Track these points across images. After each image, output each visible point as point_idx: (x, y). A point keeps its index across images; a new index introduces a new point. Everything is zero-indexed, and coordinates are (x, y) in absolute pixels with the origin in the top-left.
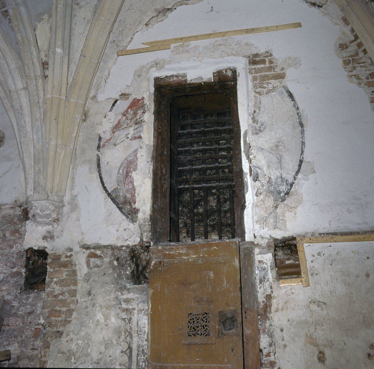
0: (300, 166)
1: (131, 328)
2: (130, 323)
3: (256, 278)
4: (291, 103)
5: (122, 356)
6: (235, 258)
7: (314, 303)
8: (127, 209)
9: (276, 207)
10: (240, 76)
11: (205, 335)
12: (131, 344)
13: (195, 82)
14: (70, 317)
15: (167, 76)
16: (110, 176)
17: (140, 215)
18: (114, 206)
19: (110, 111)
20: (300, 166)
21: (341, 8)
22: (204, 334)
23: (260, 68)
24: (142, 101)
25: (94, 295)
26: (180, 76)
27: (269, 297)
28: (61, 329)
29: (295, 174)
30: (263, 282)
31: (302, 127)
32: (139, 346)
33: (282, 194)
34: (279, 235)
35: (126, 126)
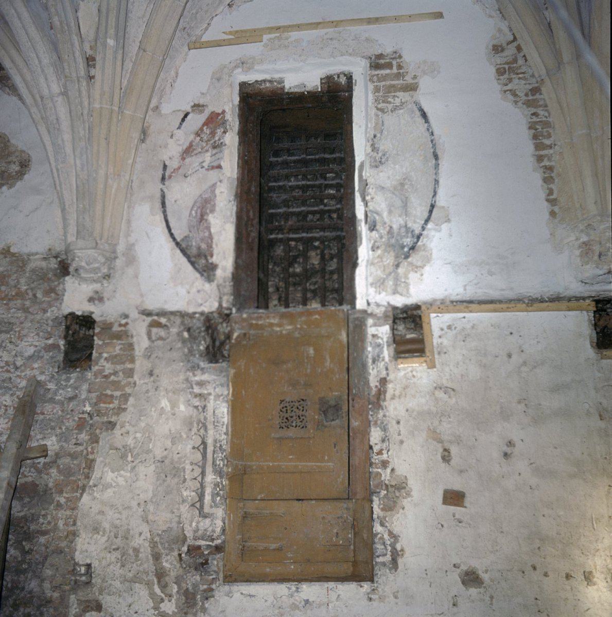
0: (431, 212)
1: (205, 419)
7: (441, 388)
9: (397, 266)
13: (296, 90)
15: (257, 81)
17: (219, 272)
20: (431, 212)
26: (275, 81)
27: (383, 381)
28: (113, 419)
32: (215, 441)
33: (406, 249)
34: (399, 301)
35: (200, 150)
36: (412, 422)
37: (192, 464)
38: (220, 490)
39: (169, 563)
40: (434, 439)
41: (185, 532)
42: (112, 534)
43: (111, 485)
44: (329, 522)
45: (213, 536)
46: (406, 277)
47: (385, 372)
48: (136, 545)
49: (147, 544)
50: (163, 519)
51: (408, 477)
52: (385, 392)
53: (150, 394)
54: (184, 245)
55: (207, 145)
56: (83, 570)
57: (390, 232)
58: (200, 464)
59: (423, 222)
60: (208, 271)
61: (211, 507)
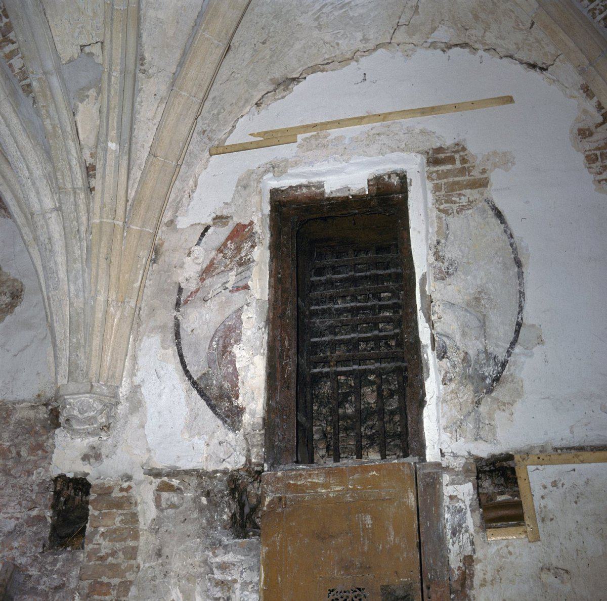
0: (517, 332)
3: (445, 527)
4: (499, 228)
6: (409, 491)
7: (549, 570)
8: (225, 408)
9: (478, 403)
13: (338, 195)
17: (246, 418)
18: (202, 403)
19: (198, 244)
20: (517, 332)
23: (445, 171)
25: (167, 556)
26: (314, 186)
27: (469, 561)
29: (508, 346)
31: (519, 267)
33: (488, 381)
34: (484, 450)
46: (491, 418)
52: (472, 576)
55: (231, 262)
57: (466, 359)
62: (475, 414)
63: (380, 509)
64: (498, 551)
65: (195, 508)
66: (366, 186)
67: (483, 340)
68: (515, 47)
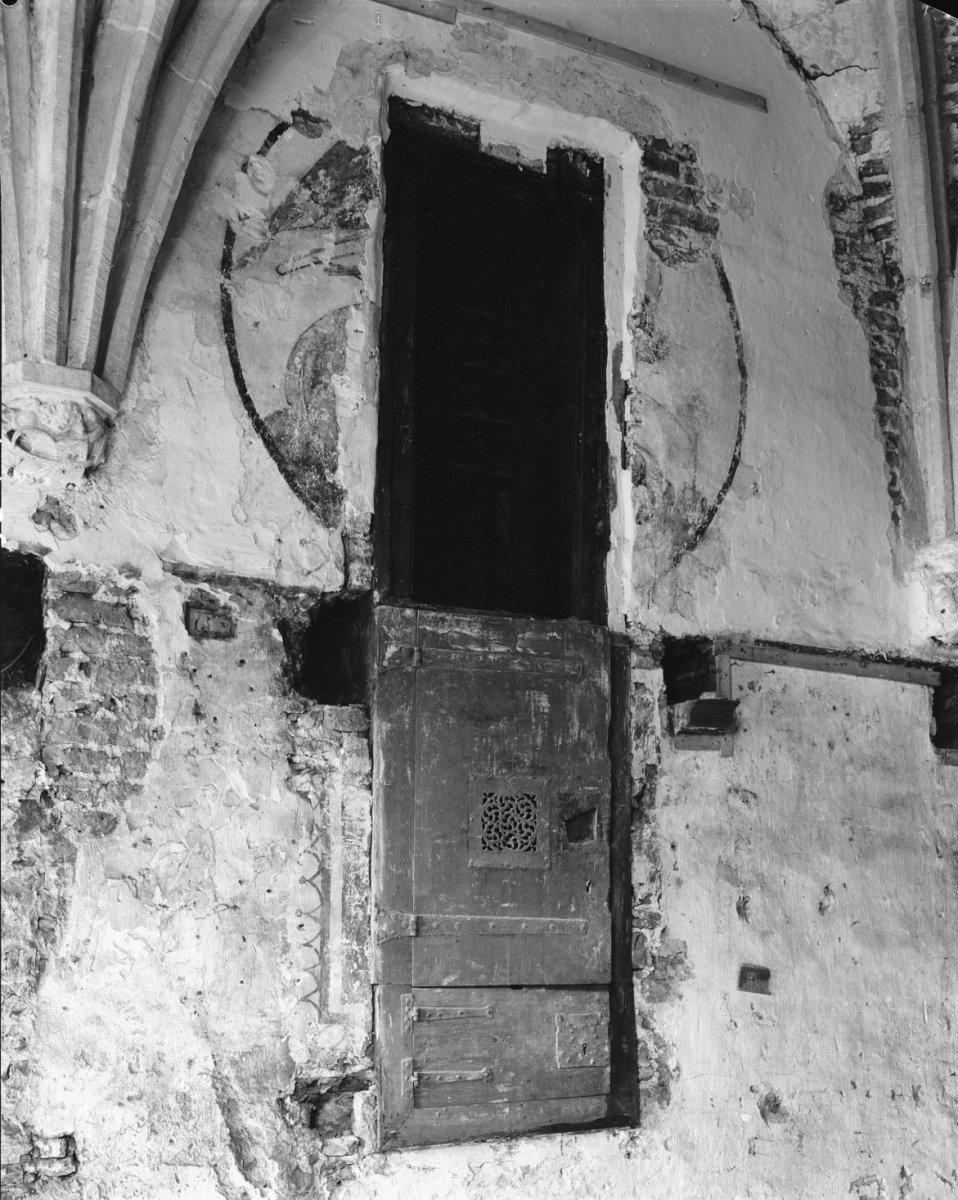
0: (733, 471)
1: (325, 820)
2: (322, 806)
3: (630, 724)
4: (723, 308)
5: (302, 892)
6: (602, 668)
7: (737, 791)
8: (311, 483)
9: (677, 560)
10: (612, 186)
11: (525, 847)
12: (327, 861)
13: (501, 155)
14: (140, 775)
15: (424, 106)
16: (265, 368)
17: (348, 506)
18: (272, 465)
19: (262, 153)
20: (733, 471)
21: (909, 108)
22: (522, 847)
23: (665, 184)
24: (360, 157)
25: (215, 719)
26: (459, 121)
27: (651, 771)
28: (110, 808)
29: (720, 488)
30: (642, 735)
31: (742, 377)
32: (347, 867)
33: (691, 532)
34: (678, 628)
35: (311, 220)
36: (695, 847)
37: (299, 913)
38: (359, 967)
39: (259, 1120)
40: (727, 879)
41: (292, 1054)
42: (124, 1065)
43: (116, 959)
44: (571, 1025)
45: (345, 1058)
46: (690, 584)
47: (655, 756)
48: (182, 1087)
49: (207, 1083)
50: (238, 1028)
51: (688, 944)
52: (653, 791)
53: (199, 758)
54: (273, 432)
55: (327, 213)
56: (56, 1149)
57: (668, 494)
58: (318, 914)
59: (720, 488)
60: (323, 500)
61: (343, 1001)
62: (673, 574)
63: (561, 687)
64: (685, 762)
65: (262, 646)
66: (544, 158)
67: (692, 471)
68: (789, 18)
